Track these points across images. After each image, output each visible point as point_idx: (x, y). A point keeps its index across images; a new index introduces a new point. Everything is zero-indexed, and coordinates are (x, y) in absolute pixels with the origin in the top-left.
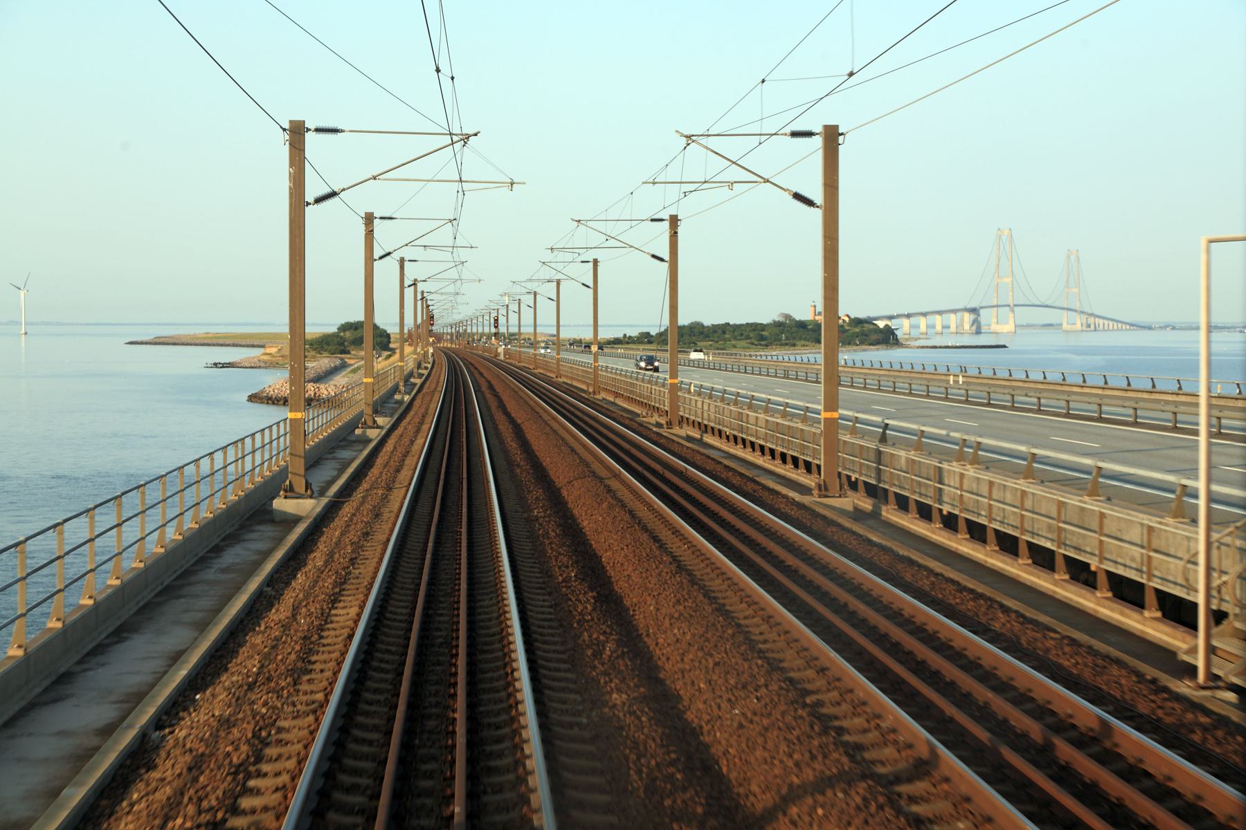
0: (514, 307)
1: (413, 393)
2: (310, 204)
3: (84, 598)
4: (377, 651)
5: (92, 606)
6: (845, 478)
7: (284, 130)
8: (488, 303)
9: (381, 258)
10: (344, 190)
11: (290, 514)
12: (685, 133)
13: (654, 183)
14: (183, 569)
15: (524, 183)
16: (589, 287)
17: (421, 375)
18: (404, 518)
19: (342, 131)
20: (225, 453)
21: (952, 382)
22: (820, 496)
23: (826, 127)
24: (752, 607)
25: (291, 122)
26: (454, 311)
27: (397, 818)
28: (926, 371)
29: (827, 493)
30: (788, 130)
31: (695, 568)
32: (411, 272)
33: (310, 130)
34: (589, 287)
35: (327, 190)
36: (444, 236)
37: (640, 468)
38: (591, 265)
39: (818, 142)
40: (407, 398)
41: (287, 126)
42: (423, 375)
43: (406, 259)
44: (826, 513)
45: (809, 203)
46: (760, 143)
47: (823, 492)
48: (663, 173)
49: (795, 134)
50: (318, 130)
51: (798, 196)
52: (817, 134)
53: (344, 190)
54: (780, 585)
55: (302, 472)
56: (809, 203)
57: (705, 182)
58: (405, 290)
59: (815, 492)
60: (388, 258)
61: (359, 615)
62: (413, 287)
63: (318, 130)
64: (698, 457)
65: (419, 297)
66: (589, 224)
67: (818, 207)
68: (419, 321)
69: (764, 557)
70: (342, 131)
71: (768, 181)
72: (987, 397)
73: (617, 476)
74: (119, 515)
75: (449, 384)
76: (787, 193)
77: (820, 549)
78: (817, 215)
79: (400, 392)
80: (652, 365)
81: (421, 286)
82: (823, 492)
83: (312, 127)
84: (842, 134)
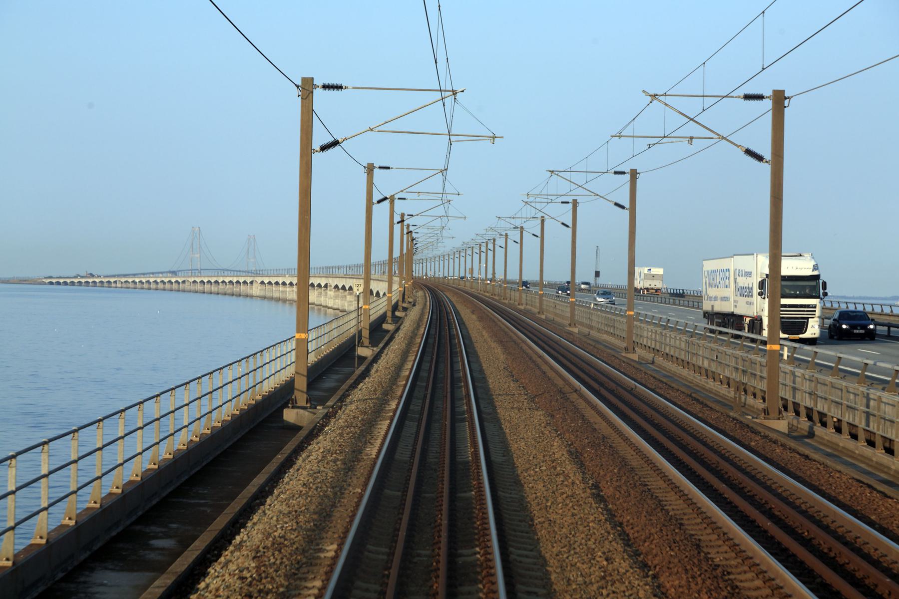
0: (501, 242)
1: (381, 345)
2: (317, 151)
5: (73, 526)
7: (298, 86)
8: (474, 236)
9: (324, 148)
10: (346, 139)
11: (290, 422)
13: (620, 137)
14: (121, 528)
15: (502, 137)
16: (537, 236)
26: (439, 244)
30: (742, 92)
32: (384, 184)
33: (318, 87)
34: (537, 236)
35: (330, 140)
36: (435, 184)
39: (768, 104)
41: (299, 83)
45: (623, 207)
46: (704, 110)
49: (747, 97)
50: (380, 168)
51: (616, 204)
53: (346, 139)
55: (305, 390)
56: (623, 207)
57: (665, 137)
60: (336, 149)
62: (400, 224)
63: (380, 168)
64: (788, 455)
65: (405, 232)
66: (561, 174)
67: (766, 162)
73: (524, 342)
75: (435, 308)
76: (739, 149)
77: (683, 415)
78: (570, 231)
80: (566, 292)
81: (399, 207)
83: (320, 84)
84: (639, 173)
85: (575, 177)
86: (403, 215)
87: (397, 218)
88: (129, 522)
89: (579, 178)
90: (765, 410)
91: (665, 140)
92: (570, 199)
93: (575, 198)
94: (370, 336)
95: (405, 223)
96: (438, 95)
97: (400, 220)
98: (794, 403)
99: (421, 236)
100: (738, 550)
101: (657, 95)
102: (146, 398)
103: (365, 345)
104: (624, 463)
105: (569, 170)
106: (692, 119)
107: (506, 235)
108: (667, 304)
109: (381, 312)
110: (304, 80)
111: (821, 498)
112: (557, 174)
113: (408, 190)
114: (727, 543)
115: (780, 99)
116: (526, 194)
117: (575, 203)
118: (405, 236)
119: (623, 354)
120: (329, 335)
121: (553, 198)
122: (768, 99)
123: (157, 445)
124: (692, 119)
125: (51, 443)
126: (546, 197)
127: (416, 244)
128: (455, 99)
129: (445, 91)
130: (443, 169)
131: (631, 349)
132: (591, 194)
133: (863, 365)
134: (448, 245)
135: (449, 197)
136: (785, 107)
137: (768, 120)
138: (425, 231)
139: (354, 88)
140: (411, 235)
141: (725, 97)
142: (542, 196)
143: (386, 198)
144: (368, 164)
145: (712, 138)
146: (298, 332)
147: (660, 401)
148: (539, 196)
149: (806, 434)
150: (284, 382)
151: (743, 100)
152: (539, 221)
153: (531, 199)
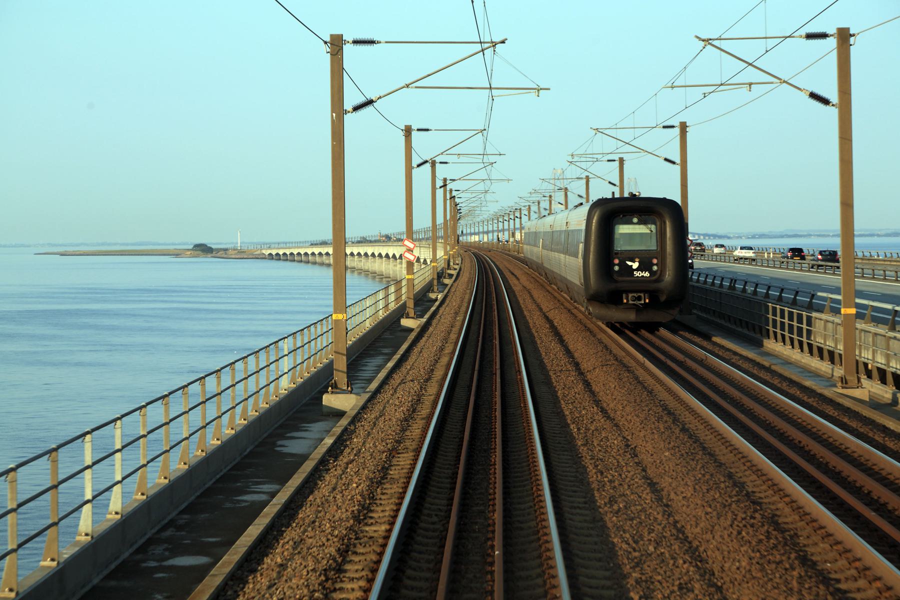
2: (349, 112)
3: (45, 560)
4: (422, 522)
6: (816, 347)
7: (326, 43)
9: (356, 108)
10: (380, 98)
12: (703, 37)
13: (672, 87)
15: (549, 89)
16: (674, 163)
17: (451, 276)
18: (451, 378)
19: (379, 42)
20: (257, 358)
21: (766, 257)
22: (843, 388)
23: (681, 123)
24: (854, 565)
25: (405, 126)
26: (483, 209)
27: (452, 591)
28: (865, 258)
29: (846, 386)
30: (803, 32)
31: (762, 495)
32: (423, 147)
33: (348, 42)
34: (674, 163)
37: (662, 357)
38: (677, 131)
40: (440, 296)
42: (453, 275)
43: (414, 127)
44: (847, 403)
45: (825, 101)
47: (844, 385)
48: (682, 77)
49: (810, 36)
50: (356, 42)
51: (814, 96)
52: (832, 35)
53: (380, 98)
54: (829, 491)
56: (825, 101)
57: (722, 85)
58: (348, 118)
59: (839, 384)
60: (369, 109)
61: (389, 531)
62: (442, 189)
63: (356, 42)
67: (833, 105)
68: (440, 220)
69: (710, 388)
70: (379, 42)
71: (784, 82)
72: (884, 275)
74: (233, 377)
75: (479, 291)
77: (840, 434)
79: (335, 386)
81: (442, 172)
82: (844, 385)
83: (439, 162)
84: (854, 35)
85: (620, 134)
86: (445, 180)
87: (439, 183)
88: (154, 531)
89: (626, 136)
90: (842, 378)
91: (722, 88)
92: (616, 157)
93: (621, 156)
94: (348, 368)
95: (448, 187)
96: (478, 47)
97: (442, 184)
98: (808, 344)
99: (463, 200)
100: (802, 513)
101: (710, 40)
102: (63, 442)
103: (410, 316)
104: (773, 521)
105: (615, 127)
106: (750, 64)
107: (550, 196)
108: (718, 261)
109: (427, 280)
110: (406, 126)
111: (883, 454)
112: (602, 132)
113: (464, 178)
114: (835, 547)
115: (844, 36)
116: (571, 154)
117: (621, 161)
118: (448, 202)
119: (840, 391)
120: (268, 372)
121: (599, 156)
122: (832, 38)
123: (187, 441)
124: (750, 64)
125: (124, 419)
126: (591, 156)
127: (460, 209)
128: (494, 51)
129: (484, 43)
130: (483, 129)
131: (852, 379)
132: (639, 150)
133: (893, 312)
134: (492, 208)
135: (492, 159)
136: (851, 45)
137: (833, 60)
138: (469, 195)
139: (386, 42)
140: (454, 200)
141: (789, 37)
142: (587, 156)
143: (426, 162)
144: (332, 36)
145: (772, 83)
146: (336, 311)
147: (763, 390)
148: (585, 156)
149: (889, 402)
150: (119, 517)
151: (805, 39)
152: (584, 181)
153: (576, 159)
